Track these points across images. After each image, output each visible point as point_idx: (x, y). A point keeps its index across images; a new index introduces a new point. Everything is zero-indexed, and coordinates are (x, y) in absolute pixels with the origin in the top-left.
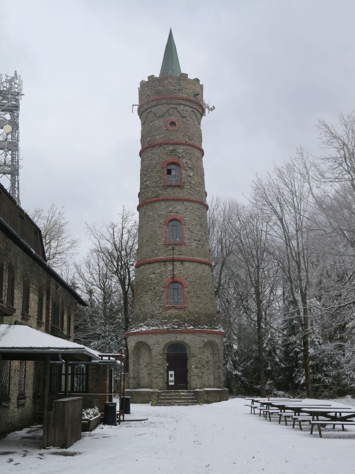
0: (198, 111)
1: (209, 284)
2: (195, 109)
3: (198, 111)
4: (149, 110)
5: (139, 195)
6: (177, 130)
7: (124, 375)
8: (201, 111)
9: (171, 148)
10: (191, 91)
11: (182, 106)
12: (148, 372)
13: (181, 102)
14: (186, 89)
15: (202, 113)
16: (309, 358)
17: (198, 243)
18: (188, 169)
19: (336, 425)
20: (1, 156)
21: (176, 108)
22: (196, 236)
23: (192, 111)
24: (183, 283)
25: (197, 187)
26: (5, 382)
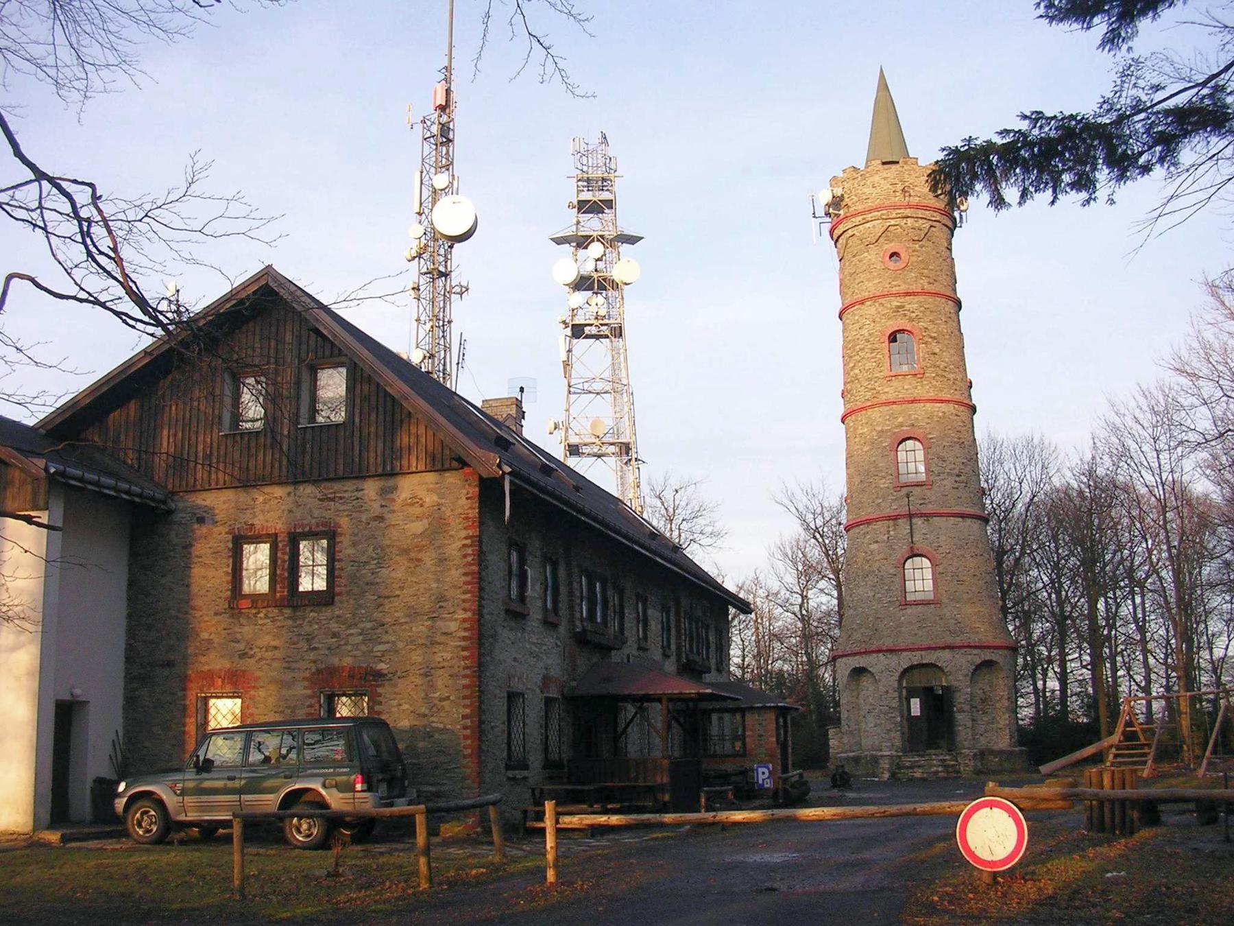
1: (982, 555)
4: (850, 232)
14: (916, 186)
17: (957, 479)
18: (930, 340)
22: (950, 467)
25: (950, 372)
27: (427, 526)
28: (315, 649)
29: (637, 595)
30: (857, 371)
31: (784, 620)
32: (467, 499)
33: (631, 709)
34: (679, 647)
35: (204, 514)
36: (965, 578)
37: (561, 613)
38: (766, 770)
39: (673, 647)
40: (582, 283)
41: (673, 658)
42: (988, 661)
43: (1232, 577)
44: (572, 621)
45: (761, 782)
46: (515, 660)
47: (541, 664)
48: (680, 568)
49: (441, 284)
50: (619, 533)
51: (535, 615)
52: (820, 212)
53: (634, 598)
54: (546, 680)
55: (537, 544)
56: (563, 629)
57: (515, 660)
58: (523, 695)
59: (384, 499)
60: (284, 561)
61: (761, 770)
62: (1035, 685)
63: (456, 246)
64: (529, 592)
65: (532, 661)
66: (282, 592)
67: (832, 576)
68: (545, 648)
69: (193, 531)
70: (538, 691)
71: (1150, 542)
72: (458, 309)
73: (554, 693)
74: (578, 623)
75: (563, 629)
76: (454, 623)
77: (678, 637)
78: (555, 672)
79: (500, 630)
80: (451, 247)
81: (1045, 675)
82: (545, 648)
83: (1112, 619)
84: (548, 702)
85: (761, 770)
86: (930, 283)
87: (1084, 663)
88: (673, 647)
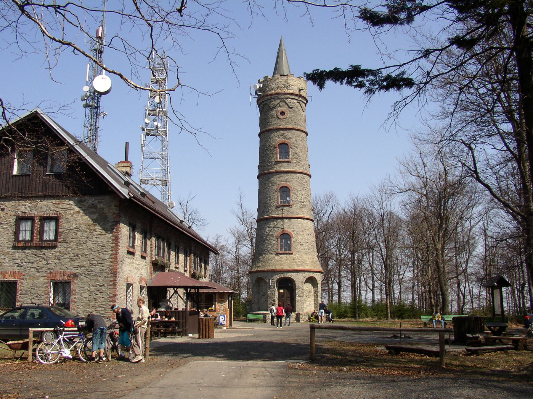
0: (303, 102)
2: (300, 100)
3: (303, 102)
5: (259, 167)
6: (286, 118)
7: (15, 191)
8: (305, 102)
9: (282, 208)
10: (296, 87)
11: (289, 100)
12: (84, 103)
13: (289, 96)
15: (306, 102)
16: (144, 302)
17: (302, 204)
19: (498, 290)
20: (11, 1)
21: (285, 102)
23: (298, 102)
24: (288, 233)
26: (219, 268)
27: (98, 216)
28: (50, 264)
29: (175, 246)
30: (264, 158)
31: (229, 257)
32: (115, 206)
33: (172, 291)
34: (190, 267)
35: (4, 207)
36: (303, 243)
37: (147, 252)
38: (223, 317)
39: (188, 267)
40: (152, 113)
41: (188, 271)
42: (308, 278)
43: (4, 398)
44: (151, 256)
45: (221, 322)
46: (130, 271)
47: (139, 273)
48: (193, 236)
49: (95, 111)
50: (170, 221)
51: (138, 253)
52: (253, 93)
53: (174, 247)
54: (141, 279)
55: (140, 225)
56: (148, 259)
57: (130, 271)
58: (132, 284)
59: (81, 205)
60: (38, 228)
61: (221, 317)
62: (328, 287)
63: (102, 96)
64: (136, 244)
65: (136, 271)
66: (36, 240)
67: (249, 239)
68: (141, 266)
69: (421, 296)
70: (138, 283)
71: (376, 232)
72: (101, 122)
73: (143, 284)
74: (153, 256)
75: (148, 259)
76: (107, 255)
77: (190, 263)
78: (144, 276)
79: (125, 258)
80: (100, 96)
81: (333, 283)
82: (141, 266)
83: (360, 262)
84: (142, 288)
85: (221, 317)
86: (296, 125)
87: (349, 278)
88: (188, 267)
